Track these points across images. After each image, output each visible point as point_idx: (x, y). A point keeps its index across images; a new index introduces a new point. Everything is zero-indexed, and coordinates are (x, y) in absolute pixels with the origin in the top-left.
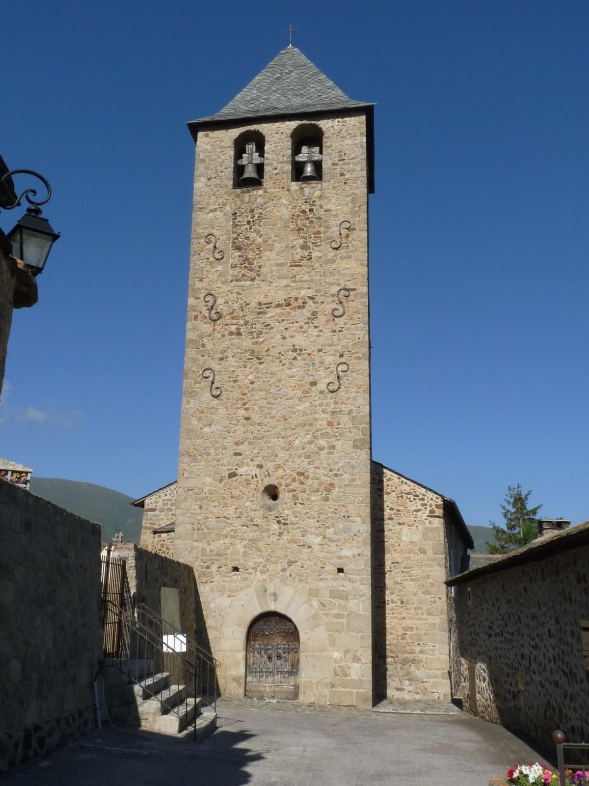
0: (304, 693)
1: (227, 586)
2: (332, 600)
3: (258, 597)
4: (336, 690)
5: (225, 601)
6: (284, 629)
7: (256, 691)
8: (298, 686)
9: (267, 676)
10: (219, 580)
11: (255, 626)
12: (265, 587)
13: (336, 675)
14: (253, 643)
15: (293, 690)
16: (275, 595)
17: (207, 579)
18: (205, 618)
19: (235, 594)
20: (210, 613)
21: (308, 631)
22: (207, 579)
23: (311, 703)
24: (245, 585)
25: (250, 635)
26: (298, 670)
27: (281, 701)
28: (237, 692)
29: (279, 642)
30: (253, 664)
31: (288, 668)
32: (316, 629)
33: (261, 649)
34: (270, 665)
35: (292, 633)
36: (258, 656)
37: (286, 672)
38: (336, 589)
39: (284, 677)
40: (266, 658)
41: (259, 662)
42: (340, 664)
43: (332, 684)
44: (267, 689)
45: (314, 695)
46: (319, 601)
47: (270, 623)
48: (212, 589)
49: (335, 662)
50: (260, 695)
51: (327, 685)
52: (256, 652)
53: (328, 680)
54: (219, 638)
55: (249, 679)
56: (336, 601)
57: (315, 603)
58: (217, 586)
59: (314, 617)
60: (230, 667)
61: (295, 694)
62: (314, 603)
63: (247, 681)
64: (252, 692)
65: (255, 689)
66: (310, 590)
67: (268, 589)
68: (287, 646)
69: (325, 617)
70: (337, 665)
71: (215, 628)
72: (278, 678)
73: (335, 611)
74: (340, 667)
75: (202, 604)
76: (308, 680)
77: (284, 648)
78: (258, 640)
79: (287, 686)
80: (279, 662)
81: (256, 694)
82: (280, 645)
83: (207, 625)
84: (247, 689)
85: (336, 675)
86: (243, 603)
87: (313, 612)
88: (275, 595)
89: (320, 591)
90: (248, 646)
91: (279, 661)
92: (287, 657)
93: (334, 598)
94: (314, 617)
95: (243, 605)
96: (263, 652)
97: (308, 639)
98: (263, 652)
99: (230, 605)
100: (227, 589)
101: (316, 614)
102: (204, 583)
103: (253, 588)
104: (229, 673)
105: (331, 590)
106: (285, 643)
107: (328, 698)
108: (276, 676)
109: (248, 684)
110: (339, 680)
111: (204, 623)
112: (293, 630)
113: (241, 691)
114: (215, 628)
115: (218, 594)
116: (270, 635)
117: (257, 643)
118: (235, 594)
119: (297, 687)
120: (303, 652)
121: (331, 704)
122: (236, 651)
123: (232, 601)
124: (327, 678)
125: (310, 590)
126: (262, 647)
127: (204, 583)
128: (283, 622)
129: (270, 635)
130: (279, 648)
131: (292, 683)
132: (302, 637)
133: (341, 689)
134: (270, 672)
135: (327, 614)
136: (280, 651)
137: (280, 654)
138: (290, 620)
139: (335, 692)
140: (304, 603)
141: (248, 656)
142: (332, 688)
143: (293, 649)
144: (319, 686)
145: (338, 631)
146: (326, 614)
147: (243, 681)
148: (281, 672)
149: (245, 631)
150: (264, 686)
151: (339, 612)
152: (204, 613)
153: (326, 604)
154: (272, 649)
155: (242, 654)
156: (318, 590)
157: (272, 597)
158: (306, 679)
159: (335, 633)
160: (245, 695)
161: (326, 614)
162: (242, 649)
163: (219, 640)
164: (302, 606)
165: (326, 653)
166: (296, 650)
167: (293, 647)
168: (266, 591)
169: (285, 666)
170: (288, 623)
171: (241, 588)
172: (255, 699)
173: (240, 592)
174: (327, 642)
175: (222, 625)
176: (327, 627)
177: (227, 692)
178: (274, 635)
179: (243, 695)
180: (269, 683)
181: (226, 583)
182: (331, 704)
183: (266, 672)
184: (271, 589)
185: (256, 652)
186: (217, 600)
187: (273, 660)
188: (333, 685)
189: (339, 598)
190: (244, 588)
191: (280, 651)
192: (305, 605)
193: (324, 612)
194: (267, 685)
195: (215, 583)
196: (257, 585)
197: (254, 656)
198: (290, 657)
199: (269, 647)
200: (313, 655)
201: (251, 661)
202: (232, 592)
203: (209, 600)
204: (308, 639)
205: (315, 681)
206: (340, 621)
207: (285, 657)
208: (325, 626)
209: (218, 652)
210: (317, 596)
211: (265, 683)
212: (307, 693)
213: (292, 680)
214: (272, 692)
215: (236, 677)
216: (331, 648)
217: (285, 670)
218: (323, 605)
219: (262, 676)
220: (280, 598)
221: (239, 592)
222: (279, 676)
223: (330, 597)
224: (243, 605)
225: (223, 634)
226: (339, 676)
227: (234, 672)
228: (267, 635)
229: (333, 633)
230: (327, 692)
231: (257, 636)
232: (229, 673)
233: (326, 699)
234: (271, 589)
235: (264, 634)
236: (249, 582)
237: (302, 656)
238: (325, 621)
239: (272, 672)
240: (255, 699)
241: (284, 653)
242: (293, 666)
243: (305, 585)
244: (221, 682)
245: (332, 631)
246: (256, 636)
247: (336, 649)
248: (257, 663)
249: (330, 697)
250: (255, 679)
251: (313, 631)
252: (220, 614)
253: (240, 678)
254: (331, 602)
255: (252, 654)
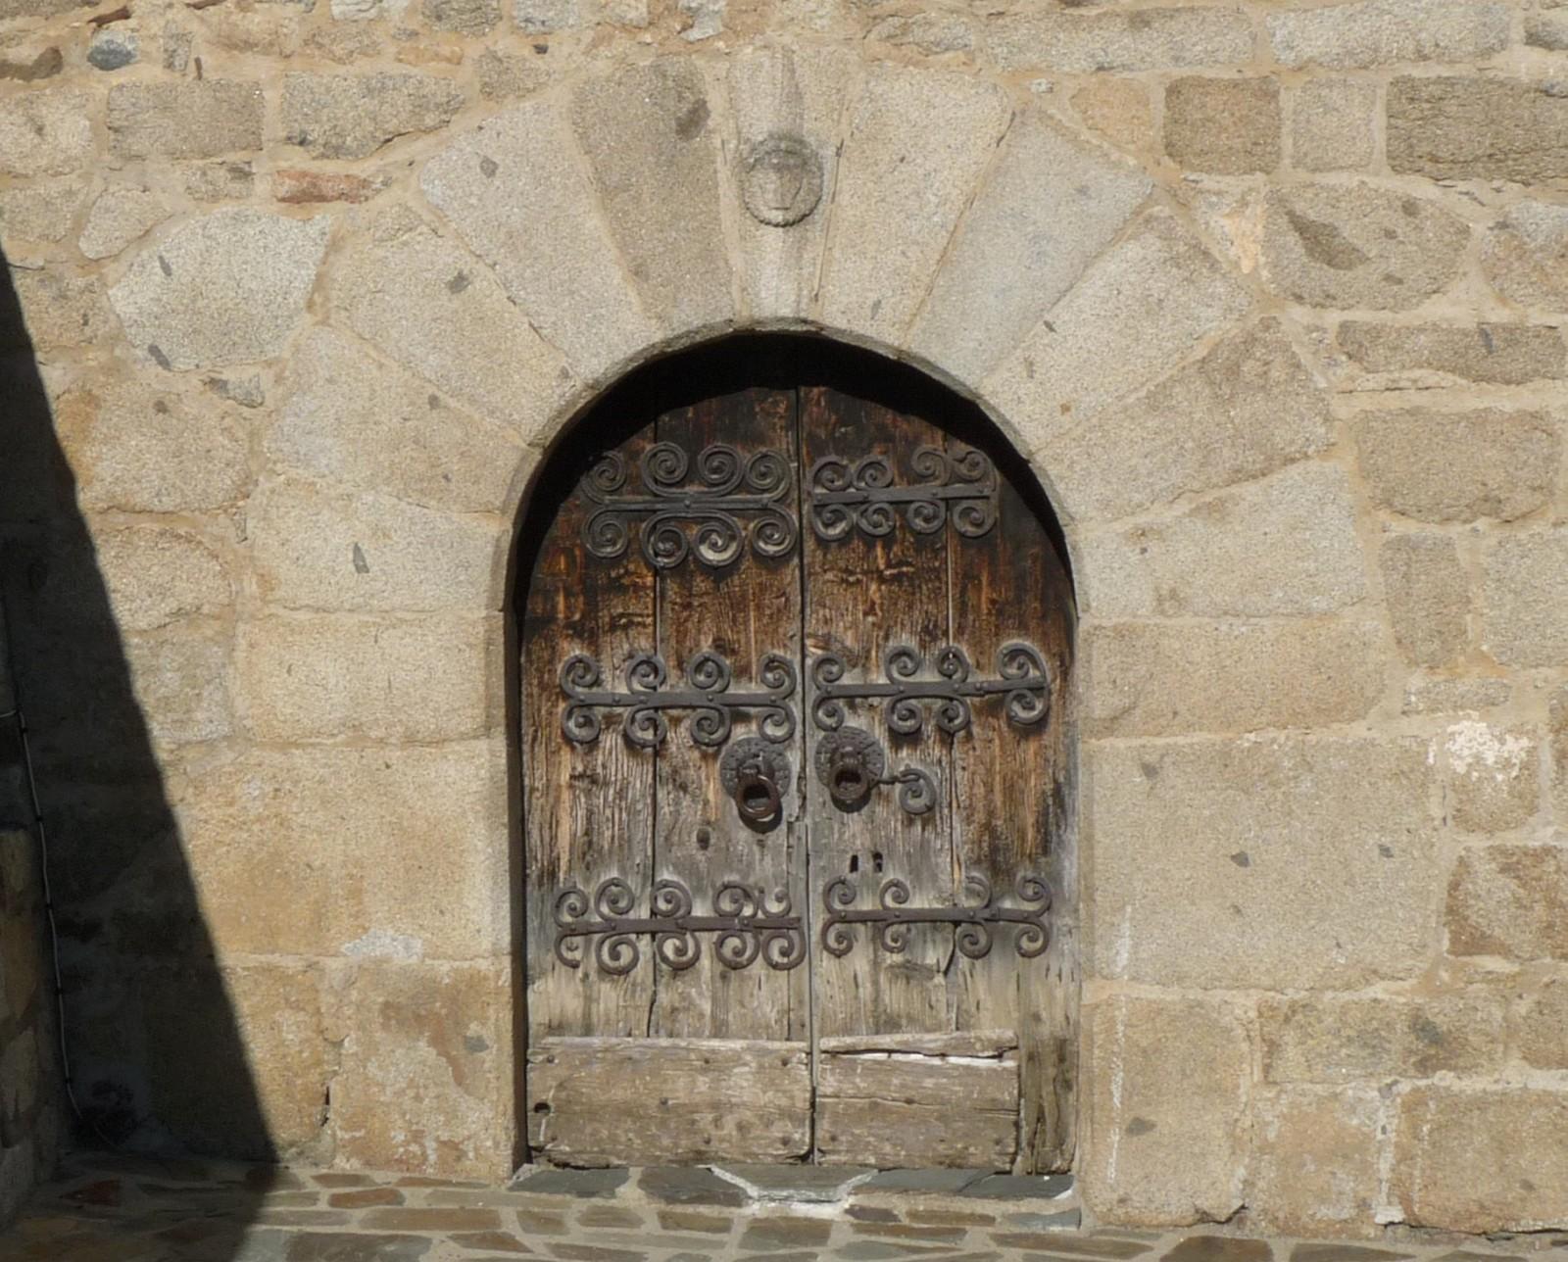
0: (1139, 1127)
1: (272, 96)
2: (1422, 189)
3: (608, 192)
4: (1471, 1085)
5: (261, 250)
6: (900, 505)
7: (626, 1111)
8: (1063, 1052)
9: (732, 966)
10: (183, 38)
11: (592, 486)
12: (687, 83)
13: (1471, 942)
14: (574, 650)
15: (1008, 1094)
16: (792, 157)
17: (54, 31)
18: (62, 427)
19: (363, 168)
20: (115, 369)
21: (1164, 515)
22: (54, 31)
23: (1204, 1217)
24: (466, 76)
25: (540, 574)
26: (1047, 893)
27: (899, 1205)
28: (437, 1128)
29: (843, 630)
30: (588, 851)
31: (947, 880)
32: (1250, 491)
33: (656, 710)
34: (765, 863)
35: (1013, 543)
36: (637, 776)
37: (932, 920)
38: (1465, 70)
39: (910, 972)
40: (713, 791)
41: (642, 833)
42: (1511, 839)
43: (1421, 1027)
44: (743, 1086)
45: (1236, 1145)
46: (1278, 201)
47: (745, 457)
48: (113, 131)
49: (1462, 819)
50: (670, 1144)
51: (1369, 1041)
52: (611, 740)
53: (1378, 990)
54: (229, 614)
55: (554, 994)
56: (1473, 204)
57: (1240, 231)
58: (164, 102)
59: (1226, 370)
60: (356, 893)
61: (1034, 1125)
62: (1229, 225)
63: (537, 1017)
64: (593, 1114)
65: (620, 1093)
66: (1173, 90)
67: (716, 100)
68: (929, 676)
69: (1346, 368)
70: (1478, 842)
71: (174, 526)
72: (843, 978)
73: (1462, 305)
74: (1512, 864)
75: (21, 284)
76: (1172, 995)
77: (898, 696)
78: (622, 625)
79: (954, 1040)
80: (855, 831)
81: (626, 1133)
82: (859, 660)
83: (87, 498)
84: (542, 1088)
85: (1471, 942)
86: (448, 257)
87: (1215, 324)
88: (792, 157)
89: (1287, 101)
90: (530, 687)
91: (855, 822)
92: (935, 775)
93: (1442, 167)
94: (1233, 371)
95: (459, 283)
96: (679, 738)
97: (1171, 599)
98: (679, 738)
99: (320, 282)
100: (273, 127)
101: (1251, 340)
102: (27, 73)
103: (559, 96)
104: (346, 954)
105: (1406, 90)
106: (906, 640)
107: (1384, 1166)
108: (826, 964)
109: (542, 1043)
110: (1505, 989)
111: (63, 479)
112: (988, 512)
113: (484, 1125)
114: (174, 526)
115: (178, 176)
116: (750, 575)
117: (615, 651)
118: (363, 168)
119: (1052, 1067)
120: (1112, 725)
121: (1414, 1225)
122: (410, 740)
123: (335, 245)
124: (1374, 973)
125: (1173, 90)
126: (676, 685)
127: (27, 73)
128: (886, 437)
129: (750, 575)
130: (852, 698)
131: (994, 1028)
132: (1108, 580)
133: (1516, 1075)
134: (767, 928)
135: (1375, 333)
136: (853, 721)
137: (864, 749)
138: (959, 415)
139: (1457, 1108)
140: (1118, 236)
141: (535, 777)
142: (1425, 1066)
143: (994, 702)
144: (1292, 1053)
145: (1490, 504)
146: (1354, 344)
147: (494, 1024)
148: (879, 922)
149: (487, 535)
150: (709, 1063)
151: (1499, 315)
152: (55, 377)
153: (1350, 232)
154: (774, 708)
155: (473, 768)
156: (1266, 92)
157: (768, 186)
158: (1151, 993)
159: (1455, 530)
160: (525, 1152)
161: (1354, 344)
162: (471, 716)
163: (228, 639)
164: (1088, 261)
165: (1358, 730)
166: (1031, 709)
167: (991, 677)
168: (692, 121)
169: (920, 863)
170: (935, 447)
171: (421, 104)
172: (630, 1194)
173: (418, 147)
174: (1375, 624)
175: (244, 489)
176: (1365, 474)
177: (336, 1130)
178: (791, 573)
179: (506, 1153)
180: (755, 1030)
181: (256, 68)
182: (1414, 1225)
183: (723, 925)
184: (748, 103)
185: (611, 740)
186: (182, 242)
187: (790, 805)
188: (1435, 1045)
189: (1499, 162)
190: (452, 107)
191: (853, 721)
192: (1132, 250)
193: (1333, 318)
194: (738, 1052)
195: (146, 73)
196: (602, 66)
197: (591, 780)
198: (960, 773)
199: (739, 689)
200: (1225, 756)
201: (568, 828)
202: (334, 151)
203: (89, 248)
204: (1171, 599)
205: (1244, 1005)
206: (1506, 400)
207: (910, 779)
208: (1344, 463)
209: (227, 757)
210: (1259, 156)
211: (720, 1031)
212: (1166, 1119)
213: (992, 998)
214: (787, 1114)
215: (428, 988)
216: (1417, 680)
217: (919, 902)
218: (1319, 241)
219: (682, 968)
220: (849, 193)
221: (399, 153)
222: (860, 960)
223: (1402, 160)
224: (459, 283)
225: (266, 581)
226: (1505, 951)
227: (395, 944)
228: (719, 573)
229: (1434, 530)
230: (1372, 1105)
231: (617, 587)
232: (346, 954)
233: (1365, 1169)
234: (748, 103)
235: (687, 567)
236: (503, 42)
237: (1110, 780)
238: (1342, 410)
239: (781, 925)
240: (630, 1194)
241: (899, 739)
242: (994, 860)
243: (1120, 45)
244: (272, 1042)
245: (1420, 512)
246: (598, 583)
247: (1470, 682)
248: (624, 844)
249: (1405, 1156)
250: (609, 995)
251: (1216, 511)
252: (216, 384)
253: (463, 994)
254: (1410, 208)
255: (568, 763)
